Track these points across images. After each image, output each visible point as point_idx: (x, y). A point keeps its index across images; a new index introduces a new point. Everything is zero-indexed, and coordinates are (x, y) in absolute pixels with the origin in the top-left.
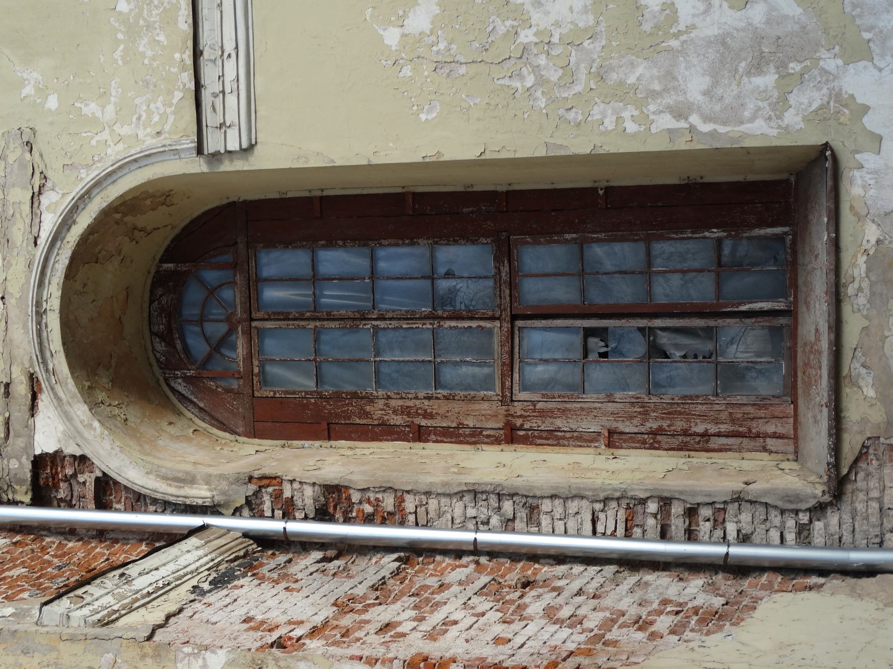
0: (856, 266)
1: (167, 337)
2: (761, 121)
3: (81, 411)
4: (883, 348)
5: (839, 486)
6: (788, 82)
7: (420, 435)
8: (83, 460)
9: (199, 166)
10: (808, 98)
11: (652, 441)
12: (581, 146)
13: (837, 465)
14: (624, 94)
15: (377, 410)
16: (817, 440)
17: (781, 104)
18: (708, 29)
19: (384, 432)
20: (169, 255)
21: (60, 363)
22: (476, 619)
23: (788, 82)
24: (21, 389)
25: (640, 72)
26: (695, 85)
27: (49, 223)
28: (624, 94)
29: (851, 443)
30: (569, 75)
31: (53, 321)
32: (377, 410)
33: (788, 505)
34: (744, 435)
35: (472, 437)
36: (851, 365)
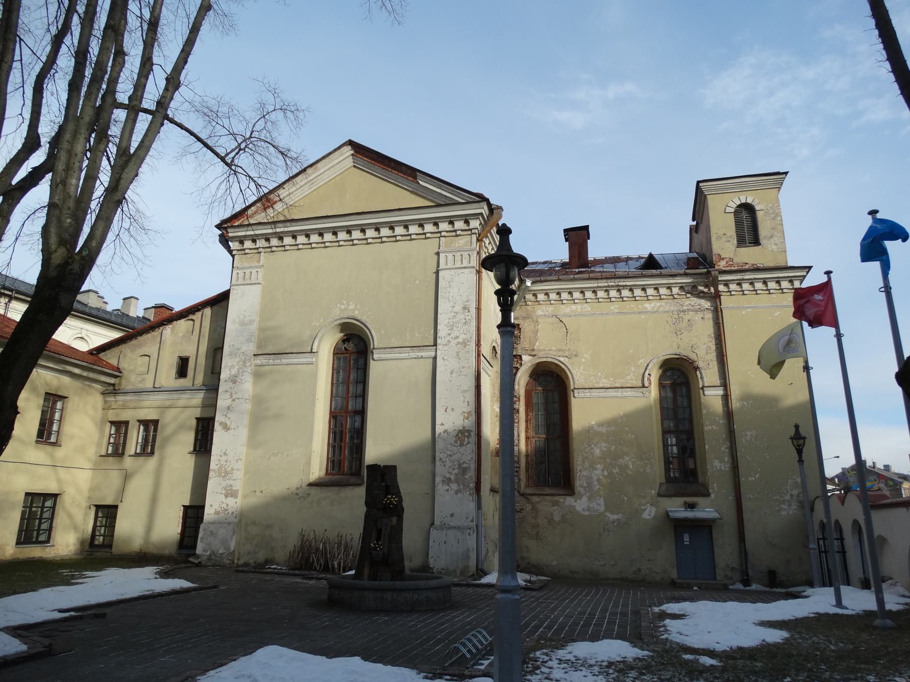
0: (556, 498)
1: (543, 374)
2: (579, 483)
3: (530, 364)
4: (515, 374)
5: (522, 495)
6: (585, 488)
7: (527, 422)
8: (521, 365)
9: (572, 388)
10: (582, 491)
11: (527, 462)
12: (575, 454)
13: (543, 587)
14: (583, 461)
15: (530, 414)
16: (529, 491)
17: (581, 487)
18: (593, 475)
19: (527, 415)
20: (558, 375)
21: (538, 361)
22: (482, 358)
23: (585, 488)
24: (533, 353)
25: (587, 464)
26: (584, 473)
27: (562, 359)
28: (583, 461)
29: (529, 497)
30: (586, 453)
31: (545, 360)
32: (530, 414)
33: (519, 487)
34: (528, 478)
35: (527, 432)
36: (541, 497)
